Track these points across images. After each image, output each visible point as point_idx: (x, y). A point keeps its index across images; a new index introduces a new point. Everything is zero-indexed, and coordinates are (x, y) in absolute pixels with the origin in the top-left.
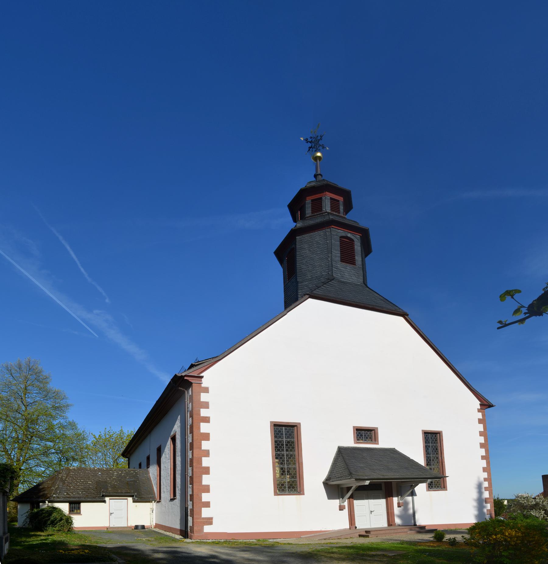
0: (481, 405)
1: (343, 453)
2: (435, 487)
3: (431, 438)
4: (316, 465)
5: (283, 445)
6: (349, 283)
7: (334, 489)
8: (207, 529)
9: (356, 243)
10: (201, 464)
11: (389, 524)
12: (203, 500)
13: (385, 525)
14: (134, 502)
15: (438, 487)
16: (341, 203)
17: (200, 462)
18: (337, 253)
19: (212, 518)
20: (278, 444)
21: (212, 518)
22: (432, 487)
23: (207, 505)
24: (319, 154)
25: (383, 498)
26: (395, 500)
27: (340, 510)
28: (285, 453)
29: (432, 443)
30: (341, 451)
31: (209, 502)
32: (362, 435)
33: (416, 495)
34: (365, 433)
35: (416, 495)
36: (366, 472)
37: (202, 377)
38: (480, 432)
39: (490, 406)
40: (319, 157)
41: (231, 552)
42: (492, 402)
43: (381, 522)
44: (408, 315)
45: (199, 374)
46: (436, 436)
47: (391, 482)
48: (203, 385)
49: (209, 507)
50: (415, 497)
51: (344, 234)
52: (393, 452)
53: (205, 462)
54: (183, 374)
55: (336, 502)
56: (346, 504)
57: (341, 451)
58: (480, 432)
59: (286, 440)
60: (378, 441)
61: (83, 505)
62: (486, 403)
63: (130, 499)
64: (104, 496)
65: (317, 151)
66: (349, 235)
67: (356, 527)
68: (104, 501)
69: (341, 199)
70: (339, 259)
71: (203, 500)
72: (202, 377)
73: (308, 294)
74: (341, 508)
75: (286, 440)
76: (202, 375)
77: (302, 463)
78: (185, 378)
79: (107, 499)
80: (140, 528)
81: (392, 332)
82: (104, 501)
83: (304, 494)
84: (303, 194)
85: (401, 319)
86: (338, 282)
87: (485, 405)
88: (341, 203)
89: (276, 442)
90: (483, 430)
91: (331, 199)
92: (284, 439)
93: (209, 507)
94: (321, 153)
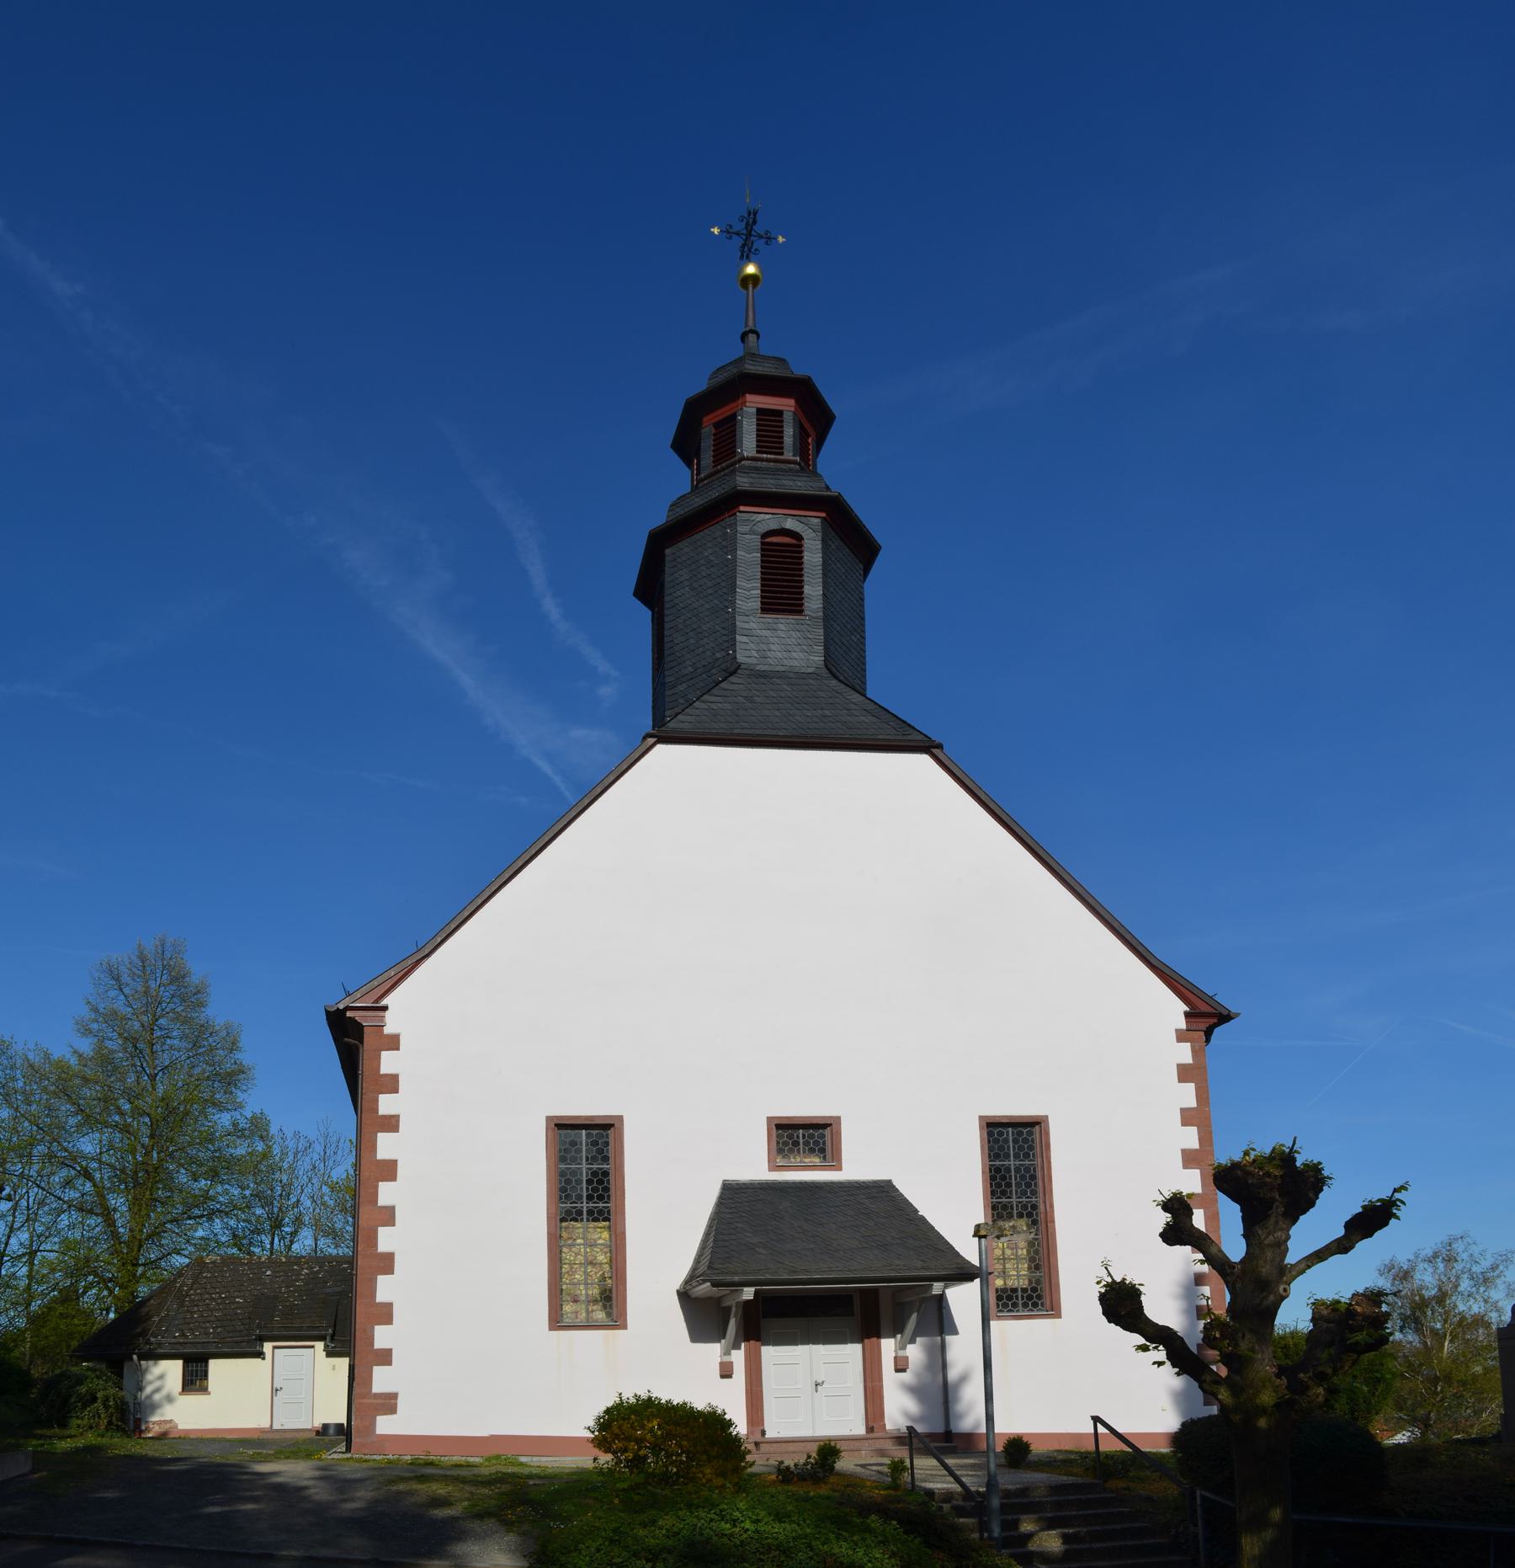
0: (1187, 1015)
1: (736, 1201)
2: (1025, 1305)
3: (1015, 1141)
4: (664, 1234)
5: (579, 1182)
6: (781, 675)
7: (706, 1311)
8: (385, 1425)
9: (807, 543)
10: (376, 1245)
11: (870, 1429)
12: (378, 1345)
13: (860, 1430)
14: (330, 1354)
15: (1035, 1305)
16: (788, 418)
17: (373, 1240)
18: (749, 591)
19: (394, 1396)
20: (568, 1182)
21: (394, 1396)
22: (1015, 1305)
23: (385, 1357)
24: (751, 269)
25: (852, 1342)
26: (888, 1346)
27: (723, 1376)
28: (1012, 1163)
29: (1016, 1156)
30: (732, 1194)
31: (390, 1351)
32: (796, 1144)
33: (955, 1332)
34: (804, 1136)
35: (955, 1332)
36: (811, 1256)
37: (385, 1008)
38: (1183, 1111)
39: (1224, 1017)
40: (754, 279)
41: (394, 1488)
42: (1228, 1002)
43: (846, 1421)
44: (940, 746)
45: (377, 1001)
46: (1030, 1133)
47: (876, 1290)
48: (387, 1030)
49: (390, 1363)
50: (949, 1338)
51: (774, 526)
52: (883, 1194)
53: (386, 1239)
54: (341, 1007)
55: (713, 1351)
56: (738, 1357)
57: (732, 1194)
58: (1183, 1111)
59: (587, 1167)
60: (839, 1160)
61: (215, 1365)
62: (1205, 1008)
63: (320, 1345)
64: (262, 1339)
65: (746, 257)
66: (790, 524)
67: (763, 1433)
68: (260, 1355)
69: (787, 405)
70: (756, 604)
71: (378, 1345)
72: (385, 1008)
73: (651, 736)
74: (726, 1372)
75: (587, 1167)
76: (384, 1002)
77: (1052, 1206)
78: (349, 1014)
79: (268, 1347)
80: (331, 1431)
81: (902, 799)
82: (260, 1355)
83: (625, 1327)
84: (695, 410)
85: (925, 759)
86: (749, 676)
87: (1206, 1018)
88: (788, 418)
89: (562, 1174)
90: (1194, 1104)
91: (760, 411)
92: (584, 1166)
93: (390, 1363)
94: (760, 266)
